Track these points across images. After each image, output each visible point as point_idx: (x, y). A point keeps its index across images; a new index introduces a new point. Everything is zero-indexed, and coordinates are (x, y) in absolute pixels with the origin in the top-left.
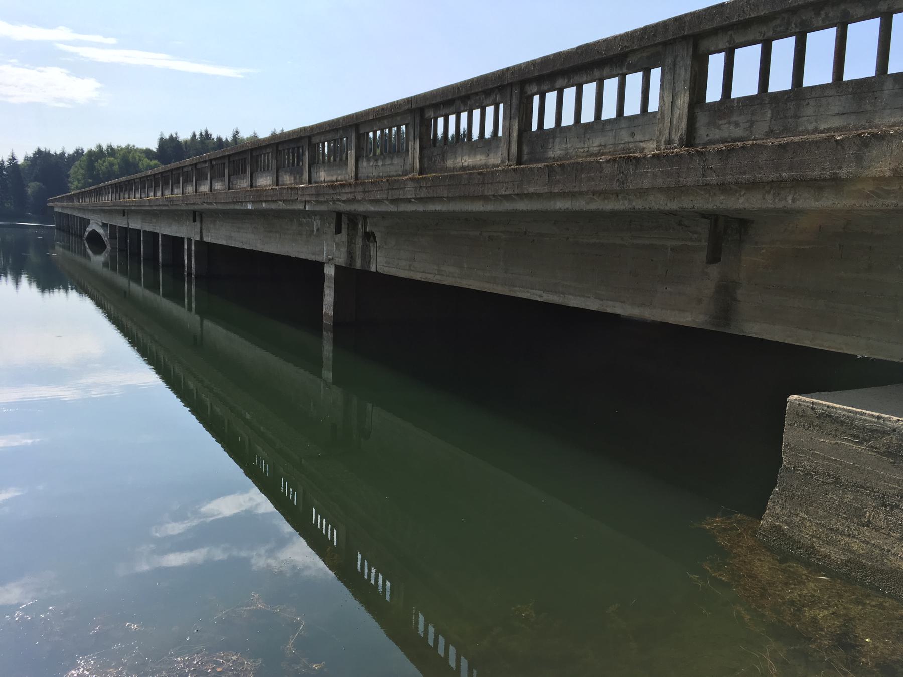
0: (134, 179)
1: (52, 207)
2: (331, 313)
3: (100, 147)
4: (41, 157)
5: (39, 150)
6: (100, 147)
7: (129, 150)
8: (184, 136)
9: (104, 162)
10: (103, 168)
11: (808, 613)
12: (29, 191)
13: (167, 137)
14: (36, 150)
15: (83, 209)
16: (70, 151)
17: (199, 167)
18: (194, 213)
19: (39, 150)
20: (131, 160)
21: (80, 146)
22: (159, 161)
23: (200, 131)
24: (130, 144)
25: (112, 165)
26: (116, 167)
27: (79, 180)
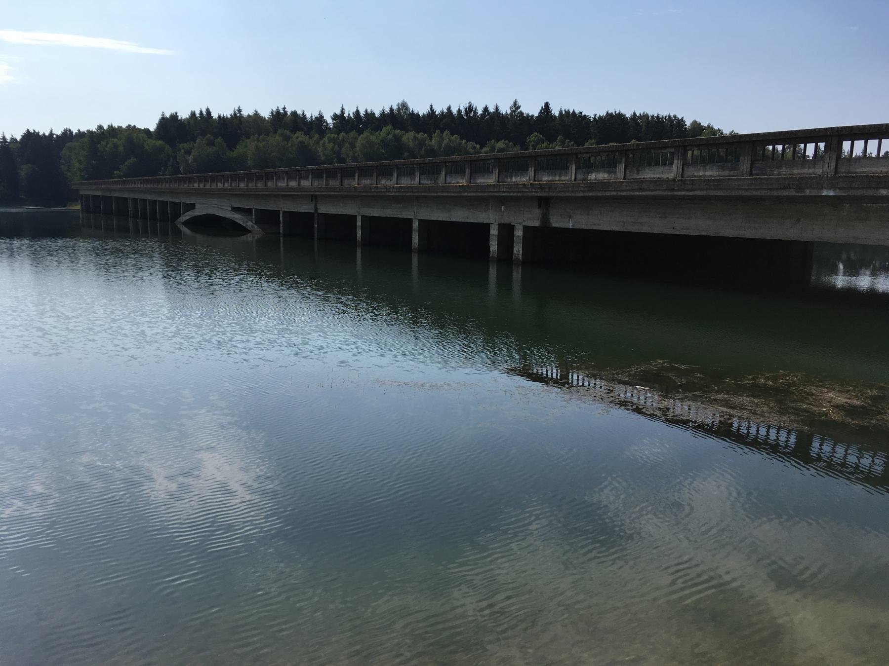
0: (239, 175)
1: (78, 190)
2: (360, 240)
3: (100, 127)
4: (30, 137)
5: (28, 131)
6: (100, 127)
7: (132, 129)
8: (184, 115)
9: (107, 143)
10: (107, 149)
11: (317, 136)
12: (23, 174)
13: (168, 115)
14: (24, 131)
15: (187, 193)
16: (58, 131)
17: (300, 172)
18: (540, 199)
19: (28, 131)
20: (135, 141)
21: (68, 128)
22: (164, 141)
23: (200, 109)
24: (130, 124)
25: (116, 146)
26: (121, 148)
27: (80, 162)
